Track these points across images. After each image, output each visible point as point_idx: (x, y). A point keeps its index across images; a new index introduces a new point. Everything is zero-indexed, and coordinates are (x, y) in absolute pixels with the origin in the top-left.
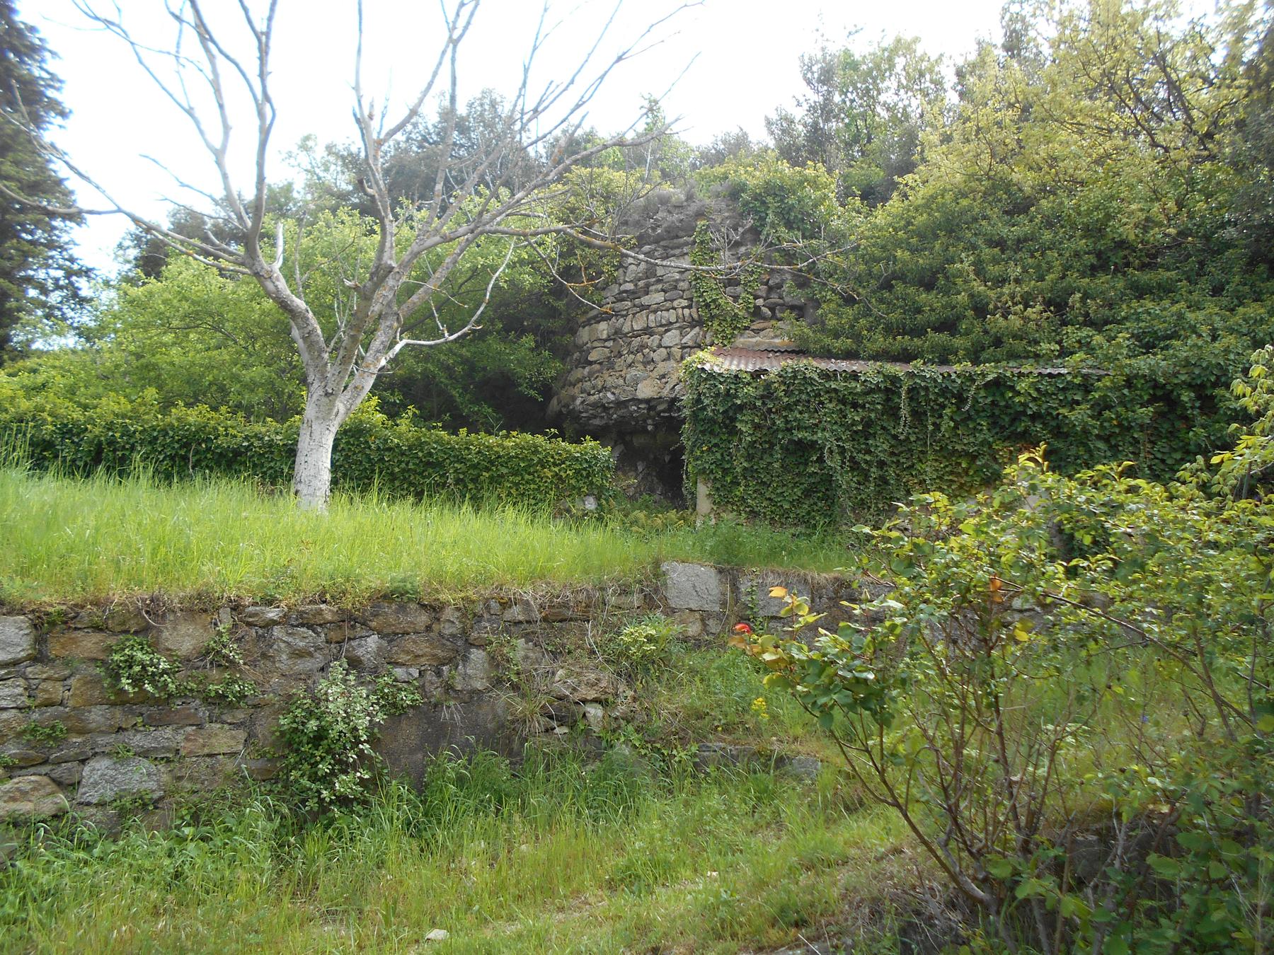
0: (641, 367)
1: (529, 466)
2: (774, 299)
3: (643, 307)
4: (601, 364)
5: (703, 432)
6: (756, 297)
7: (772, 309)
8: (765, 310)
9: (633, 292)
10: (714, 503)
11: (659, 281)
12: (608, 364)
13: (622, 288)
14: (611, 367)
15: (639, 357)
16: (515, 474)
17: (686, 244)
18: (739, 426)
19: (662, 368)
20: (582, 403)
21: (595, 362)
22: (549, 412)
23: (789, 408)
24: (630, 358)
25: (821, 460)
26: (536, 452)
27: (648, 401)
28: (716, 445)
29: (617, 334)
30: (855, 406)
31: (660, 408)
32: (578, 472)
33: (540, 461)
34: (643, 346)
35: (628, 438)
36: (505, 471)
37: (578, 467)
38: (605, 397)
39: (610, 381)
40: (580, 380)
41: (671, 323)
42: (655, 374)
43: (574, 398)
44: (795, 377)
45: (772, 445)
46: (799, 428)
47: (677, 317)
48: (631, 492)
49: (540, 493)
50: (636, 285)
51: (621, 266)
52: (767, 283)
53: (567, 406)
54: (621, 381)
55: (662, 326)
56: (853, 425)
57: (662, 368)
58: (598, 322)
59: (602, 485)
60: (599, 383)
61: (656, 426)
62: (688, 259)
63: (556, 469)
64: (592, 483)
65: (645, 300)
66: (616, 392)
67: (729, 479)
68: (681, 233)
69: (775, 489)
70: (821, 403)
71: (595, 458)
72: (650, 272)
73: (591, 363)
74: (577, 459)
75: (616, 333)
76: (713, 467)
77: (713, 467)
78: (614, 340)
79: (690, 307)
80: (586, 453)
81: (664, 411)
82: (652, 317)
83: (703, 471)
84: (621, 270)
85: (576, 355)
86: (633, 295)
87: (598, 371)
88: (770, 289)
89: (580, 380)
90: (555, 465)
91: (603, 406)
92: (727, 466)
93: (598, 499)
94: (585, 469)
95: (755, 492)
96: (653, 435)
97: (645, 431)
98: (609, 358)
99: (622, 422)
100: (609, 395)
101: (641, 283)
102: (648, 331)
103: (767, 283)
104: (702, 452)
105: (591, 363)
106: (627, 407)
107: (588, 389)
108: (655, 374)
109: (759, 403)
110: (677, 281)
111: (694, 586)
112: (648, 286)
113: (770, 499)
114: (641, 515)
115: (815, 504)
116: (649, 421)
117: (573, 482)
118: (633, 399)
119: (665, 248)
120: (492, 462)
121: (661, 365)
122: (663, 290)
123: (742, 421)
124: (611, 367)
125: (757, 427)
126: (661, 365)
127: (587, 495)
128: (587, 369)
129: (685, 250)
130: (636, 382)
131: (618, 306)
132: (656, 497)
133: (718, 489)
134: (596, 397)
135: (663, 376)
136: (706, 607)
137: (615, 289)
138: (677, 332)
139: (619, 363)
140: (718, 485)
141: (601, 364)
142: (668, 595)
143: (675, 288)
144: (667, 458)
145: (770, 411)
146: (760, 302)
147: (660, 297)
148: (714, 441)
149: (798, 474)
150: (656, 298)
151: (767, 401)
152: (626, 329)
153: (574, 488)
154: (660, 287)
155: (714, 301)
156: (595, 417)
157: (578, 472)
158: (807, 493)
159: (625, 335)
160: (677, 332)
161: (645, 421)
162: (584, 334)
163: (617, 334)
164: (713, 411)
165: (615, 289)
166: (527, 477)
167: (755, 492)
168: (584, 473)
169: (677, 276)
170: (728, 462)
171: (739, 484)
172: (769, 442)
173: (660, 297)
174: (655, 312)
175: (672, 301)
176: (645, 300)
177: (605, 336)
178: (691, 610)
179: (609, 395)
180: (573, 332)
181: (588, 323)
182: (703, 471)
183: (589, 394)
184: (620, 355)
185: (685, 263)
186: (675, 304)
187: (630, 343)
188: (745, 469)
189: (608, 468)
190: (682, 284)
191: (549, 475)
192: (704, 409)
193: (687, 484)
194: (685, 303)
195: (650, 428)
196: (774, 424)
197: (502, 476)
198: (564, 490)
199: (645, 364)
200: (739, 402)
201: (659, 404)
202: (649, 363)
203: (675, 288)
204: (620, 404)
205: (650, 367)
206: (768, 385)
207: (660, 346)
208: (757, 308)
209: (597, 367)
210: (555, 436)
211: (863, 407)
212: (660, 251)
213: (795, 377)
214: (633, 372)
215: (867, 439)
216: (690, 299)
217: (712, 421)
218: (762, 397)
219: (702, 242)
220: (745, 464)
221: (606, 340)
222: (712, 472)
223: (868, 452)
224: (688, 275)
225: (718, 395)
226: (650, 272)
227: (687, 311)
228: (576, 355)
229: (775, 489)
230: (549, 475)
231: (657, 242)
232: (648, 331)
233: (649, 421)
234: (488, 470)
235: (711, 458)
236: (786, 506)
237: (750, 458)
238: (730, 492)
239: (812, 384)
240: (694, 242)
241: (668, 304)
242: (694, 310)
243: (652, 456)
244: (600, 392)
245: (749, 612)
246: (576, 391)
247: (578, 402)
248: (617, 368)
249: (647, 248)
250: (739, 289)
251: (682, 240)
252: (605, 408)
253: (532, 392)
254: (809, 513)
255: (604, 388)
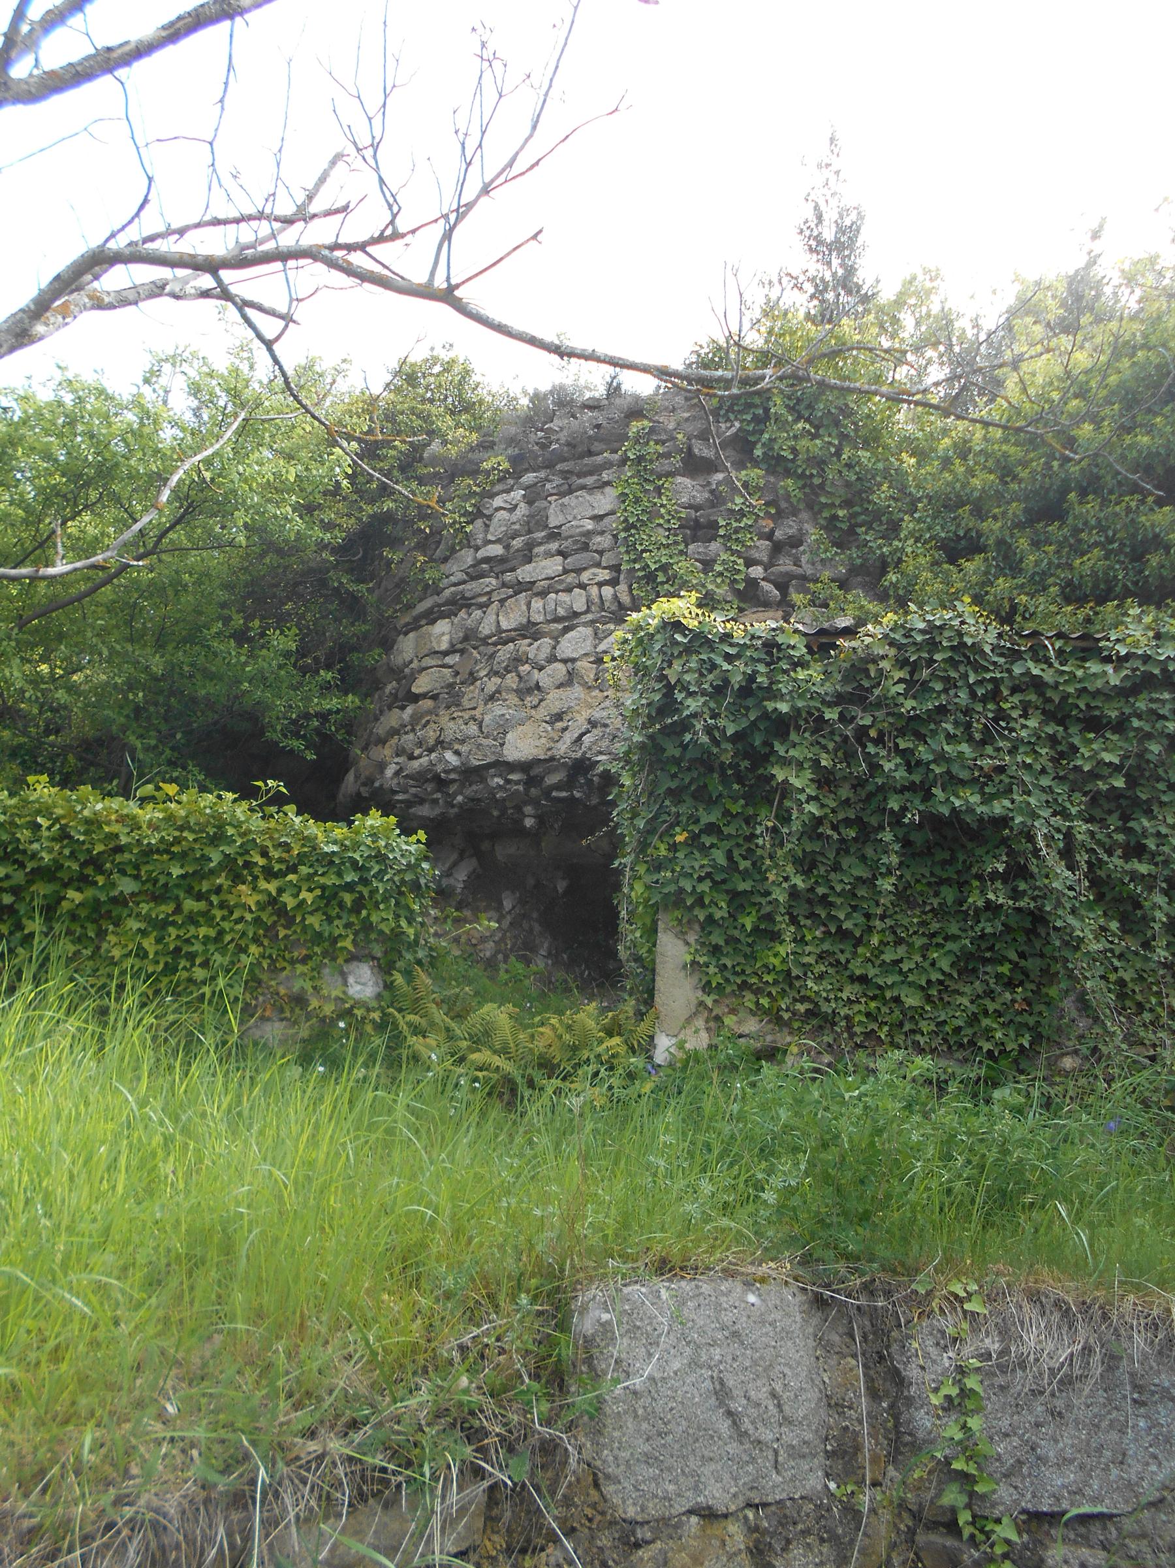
0: (513, 699)
1: (199, 875)
2: (785, 565)
3: (521, 587)
4: (435, 697)
5: (675, 795)
6: (749, 563)
7: (783, 587)
8: (767, 586)
9: (501, 560)
10: (707, 988)
11: (554, 536)
12: (450, 697)
13: (481, 554)
14: (454, 700)
15: (511, 680)
16: (157, 899)
17: (608, 465)
18: (780, 774)
19: (555, 700)
20: (397, 773)
21: (424, 696)
22: (340, 797)
23: (914, 726)
24: (492, 684)
25: (1018, 871)
26: (218, 839)
27: (524, 767)
28: (711, 829)
29: (469, 639)
30: (1094, 724)
31: (552, 779)
32: (329, 897)
33: (228, 863)
34: (518, 660)
35: (485, 846)
36: (127, 886)
37: (331, 880)
38: (441, 759)
39: (452, 729)
40: (394, 732)
41: (576, 615)
42: (542, 713)
43: (382, 766)
44: (933, 645)
45: (866, 833)
46: (952, 782)
47: (589, 602)
48: (488, 949)
49: (223, 950)
50: (507, 547)
51: (478, 514)
52: (769, 536)
53: (369, 781)
54: (473, 729)
55: (557, 620)
56: (1094, 775)
57: (555, 700)
58: (433, 622)
59: (398, 934)
60: (431, 734)
61: (541, 819)
62: (612, 493)
63: (272, 887)
64: (367, 926)
65: (525, 573)
66: (464, 749)
67: (748, 922)
68: (597, 447)
69: (878, 951)
70: (1001, 715)
71: (380, 857)
72: (536, 521)
73: (416, 698)
74: (328, 860)
75: (466, 638)
76: (705, 887)
77: (705, 887)
78: (462, 652)
79: (613, 582)
80: (356, 846)
81: (558, 787)
82: (537, 604)
83: (676, 900)
84: (479, 523)
85: (390, 688)
86: (499, 565)
87: (429, 712)
88: (777, 548)
89: (394, 732)
90: (269, 874)
91: (437, 778)
92: (743, 886)
93: (385, 968)
94: (349, 887)
95: (821, 957)
96: (534, 836)
97: (519, 831)
98: (451, 686)
99: (472, 810)
100: (449, 756)
101: (517, 543)
102: (529, 631)
103: (769, 536)
104: (674, 847)
105: (416, 698)
106: (483, 780)
107: (409, 746)
108: (542, 713)
109: (831, 715)
110: (589, 534)
111: (722, 1393)
112: (530, 546)
113: (863, 980)
114: (499, 1015)
115: (990, 994)
116: (528, 810)
117: (314, 921)
118: (496, 764)
119: (566, 474)
120: (96, 863)
121: (554, 695)
122: (560, 553)
123: (785, 762)
124: (454, 700)
125: (825, 780)
126: (554, 695)
127: (352, 958)
128: (409, 710)
129: (605, 476)
130: (503, 728)
131: (472, 587)
132: (540, 964)
133: (715, 950)
134: (424, 760)
135: (559, 717)
136: (776, 1487)
137: (467, 557)
138: (589, 631)
139: (471, 694)
140: (717, 939)
141: (435, 697)
142: (607, 1460)
143: (585, 547)
144: (561, 886)
145: (862, 732)
146: (757, 572)
147: (553, 566)
148: (707, 818)
149: (940, 913)
150: (547, 567)
151: (855, 710)
152: (486, 629)
153: (318, 937)
154: (554, 546)
155: (664, 568)
156: (422, 801)
157: (329, 897)
158: (967, 966)
159: (484, 641)
160: (589, 631)
161: (519, 809)
162: (407, 647)
163: (469, 639)
164: (709, 730)
165: (467, 557)
166: (190, 905)
167: (821, 957)
168: (348, 898)
169: (589, 525)
170: (745, 875)
171: (776, 937)
172: (859, 822)
173: (553, 566)
174: (543, 594)
175: (579, 571)
176: (525, 573)
177: (444, 646)
178: (709, 1515)
179: (449, 756)
180: (387, 645)
181: (414, 626)
182: (676, 900)
183: (412, 757)
184: (472, 678)
185: (605, 501)
186: (585, 577)
187: (492, 656)
188: (794, 893)
189: (416, 887)
190: (599, 539)
191: (251, 902)
192: (685, 725)
193: (631, 933)
194: (605, 575)
195: (529, 822)
196: (874, 767)
197: (120, 901)
198: (290, 945)
199: (522, 693)
200: (784, 707)
201: (549, 771)
202: (529, 691)
203: (585, 547)
204: (471, 774)
205: (531, 700)
206: (860, 667)
207: (552, 659)
208: (752, 583)
209: (427, 704)
210: (278, 800)
211: (1120, 726)
212: (557, 481)
213: (933, 645)
214: (498, 709)
215: (1125, 818)
216: (616, 568)
217: (706, 762)
218: (839, 699)
219: (640, 459)
220: (798, 881)
221: (446, 653)
222: (700, 902)
223: (1136, 850)
224: (612, 523)
225: (719, 691)
226: (536, 521)
227: (607, 591)
228: (390, 688)
229: (878, 951)
230: (251, 902)
231: (549, 465)
232: (529, 631)
233: (528, 810)
234: (82, 882)
235: (699, 862)
236: (912, 1000)
237: (806, 864)
238: (752, 957)
239: (978, 667)
240: (624, 461)
241: (570, 578)
242: (623, 588)
243: (531, 881)
244: (431, 750)
245: (952, 1496)
246: (387, 751)
247: (390, 772)
248: (466, 703)
249: (529, 478)
250: (715, 546)
251: (599, 459)
252: (441, 783)
253: (297, 744)
254: (974, 1020)
255: (440, 744)
